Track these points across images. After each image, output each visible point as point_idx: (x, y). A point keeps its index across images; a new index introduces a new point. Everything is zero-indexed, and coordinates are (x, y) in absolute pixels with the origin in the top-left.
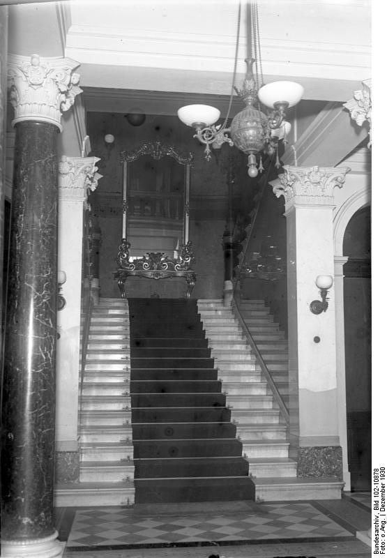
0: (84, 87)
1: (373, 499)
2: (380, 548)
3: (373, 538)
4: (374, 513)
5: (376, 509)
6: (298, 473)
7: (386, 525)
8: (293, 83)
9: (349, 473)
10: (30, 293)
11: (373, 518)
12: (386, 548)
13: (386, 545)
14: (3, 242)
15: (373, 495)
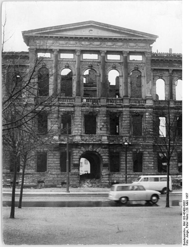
1: (183, 221)
2: (186, 243)
3: (183, 238)
5: (184, 225)
6: (110, 133)
7: (188, 234)
8: (111, 71)
9: (160, 122)
11: (183, 229)
12: (188, 242)
15: (183, 219)
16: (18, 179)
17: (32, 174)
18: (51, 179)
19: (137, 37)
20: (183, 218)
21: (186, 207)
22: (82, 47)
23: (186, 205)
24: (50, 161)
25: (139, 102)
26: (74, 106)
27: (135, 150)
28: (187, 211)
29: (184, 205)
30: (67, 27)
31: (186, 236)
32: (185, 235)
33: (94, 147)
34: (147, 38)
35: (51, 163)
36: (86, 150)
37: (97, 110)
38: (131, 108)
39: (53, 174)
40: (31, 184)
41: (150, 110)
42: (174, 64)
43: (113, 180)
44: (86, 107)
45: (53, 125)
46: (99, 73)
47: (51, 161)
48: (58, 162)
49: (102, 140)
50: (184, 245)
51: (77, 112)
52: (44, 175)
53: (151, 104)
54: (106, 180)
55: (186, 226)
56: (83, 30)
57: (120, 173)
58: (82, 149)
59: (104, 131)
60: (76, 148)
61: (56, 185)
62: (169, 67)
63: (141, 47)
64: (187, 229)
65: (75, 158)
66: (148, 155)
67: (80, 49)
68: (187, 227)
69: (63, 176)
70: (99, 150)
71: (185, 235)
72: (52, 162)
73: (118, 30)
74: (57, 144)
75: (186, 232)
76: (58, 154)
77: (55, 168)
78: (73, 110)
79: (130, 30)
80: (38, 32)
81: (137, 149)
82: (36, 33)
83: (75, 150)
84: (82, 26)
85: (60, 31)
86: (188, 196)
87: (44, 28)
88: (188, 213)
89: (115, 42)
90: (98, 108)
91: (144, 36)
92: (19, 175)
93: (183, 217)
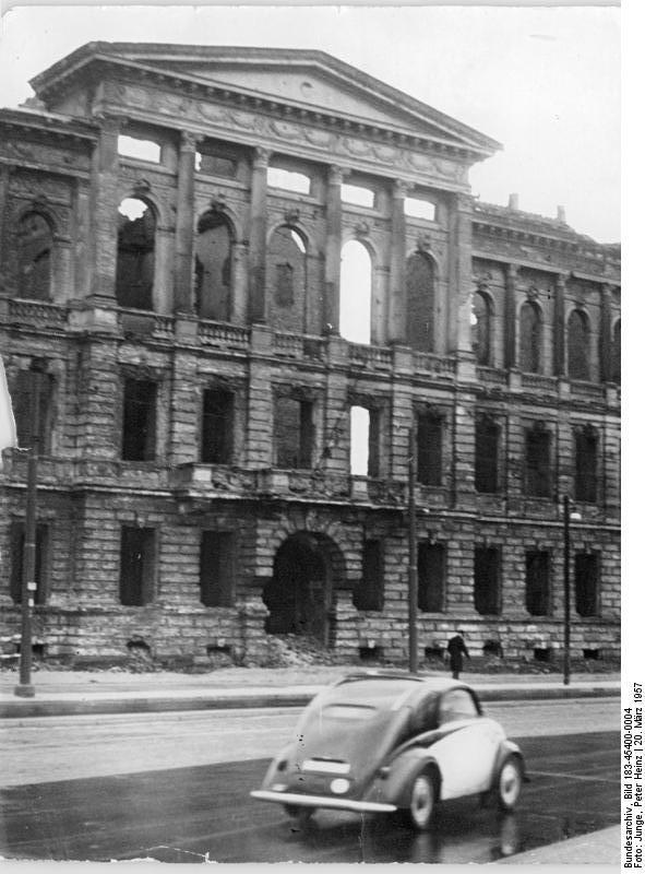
0: (519, 738)
1: (624, 781)
2: (634, 859)
3: (624, 842)
4: (625, 804)
5: (628, 797)
10: (500, 433)
11: (624, 811)
13: (643, 853)
14: (244, 74)
16: (45, 633)
17: (107, 614)
18: (173, 632)
19: (433, 134)
20: (623, 769)
21: (635, 732)
22: (276, 140)
23: (634, 724)
24: (166, 563)
25: (437, 370)
26: (247, 361)
27: (533, 543)
28: (638, 746)
29: (628, 726)
30: (242, 56)
31: (633, 836)
32: (630, 831)
33: (321, 517)
34: (469, 148)
35: (169, 572)
36: (295, 525)
37: (318, 381)
38: (416, 384)
39: (179, 615)
40: (106, 652)
41: (468, 397)
42: (524, 248)
43: (366, 639)
44: (284, 367)
45: (179, 431)
46: (318, 248)
47: (172, 564)
48: (195, 569)
49: (355, 495)
50: (628, 866)
51: (257, 382)
52: (146, 618)
53: (471, 376)
54: (348, 639)
55: (634, 799)
56: (282, 78)
57: (384, 614)
58: (282, 523)
59: (340, 459)
60: (267, 519)
61: (192, 656)
62: (510, 255)
63: (438, 171)
64: (637, 811)
65: (168, 553)
66: (460, 554)
67: (270, 148)
68: (636, 805)
69: (211, 623)
70: (333, 529)
71: (630, 831)
72: (175, 568)
73: (392, 102)
74: (207, 499)
75: (634, 820)
76: (192, 538)
77: (185, 590)
78: (242, 374)
79: (427, 110)
80: (145, 57)
81: (429, 531)
82: (138, 56)
83: (263, 527)
84: (285, 62)
85: (214, 67)
86: (643, 694)
87: (169, 46)
88: (642, 754)
89: (376, 142)
90: (319, 376)
91: (463, 138)
92: (47, 617)
93: (622, 767)
